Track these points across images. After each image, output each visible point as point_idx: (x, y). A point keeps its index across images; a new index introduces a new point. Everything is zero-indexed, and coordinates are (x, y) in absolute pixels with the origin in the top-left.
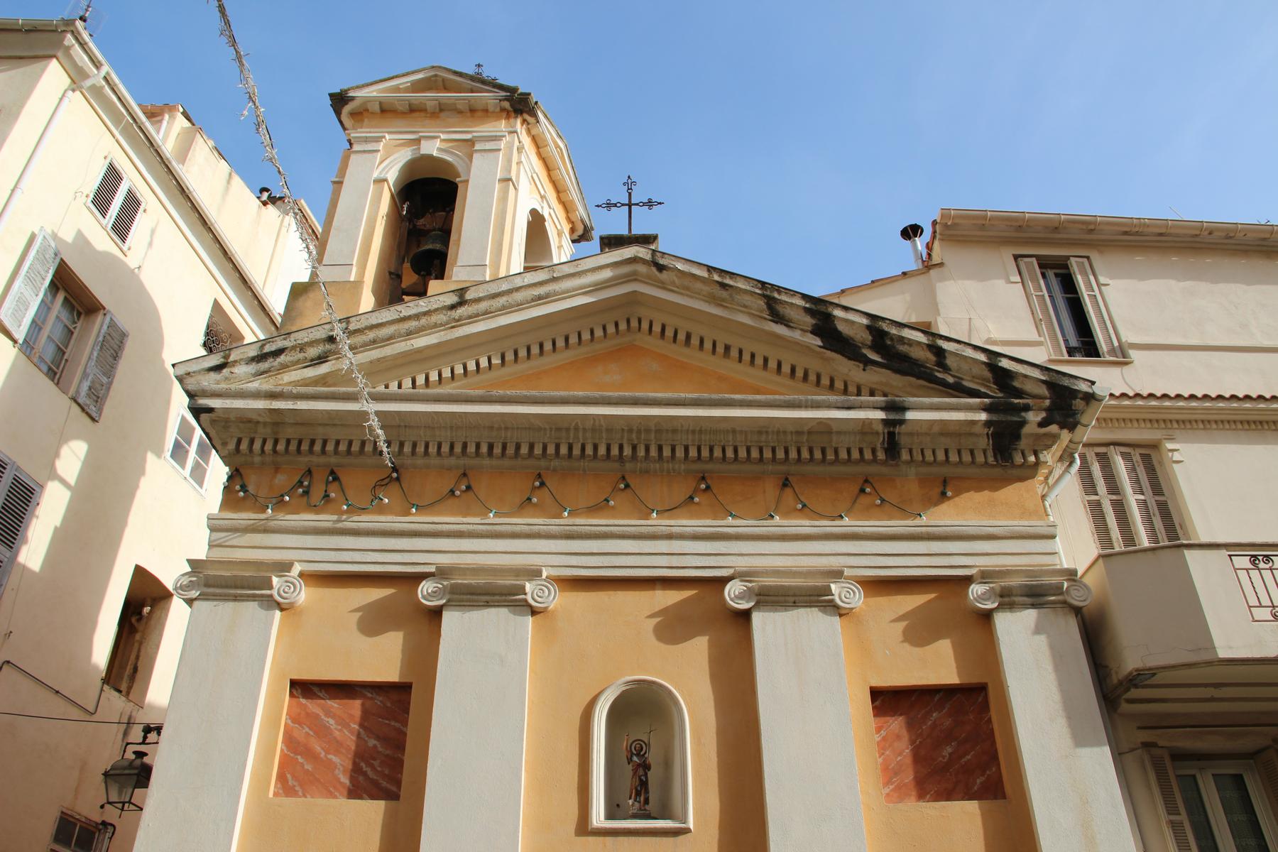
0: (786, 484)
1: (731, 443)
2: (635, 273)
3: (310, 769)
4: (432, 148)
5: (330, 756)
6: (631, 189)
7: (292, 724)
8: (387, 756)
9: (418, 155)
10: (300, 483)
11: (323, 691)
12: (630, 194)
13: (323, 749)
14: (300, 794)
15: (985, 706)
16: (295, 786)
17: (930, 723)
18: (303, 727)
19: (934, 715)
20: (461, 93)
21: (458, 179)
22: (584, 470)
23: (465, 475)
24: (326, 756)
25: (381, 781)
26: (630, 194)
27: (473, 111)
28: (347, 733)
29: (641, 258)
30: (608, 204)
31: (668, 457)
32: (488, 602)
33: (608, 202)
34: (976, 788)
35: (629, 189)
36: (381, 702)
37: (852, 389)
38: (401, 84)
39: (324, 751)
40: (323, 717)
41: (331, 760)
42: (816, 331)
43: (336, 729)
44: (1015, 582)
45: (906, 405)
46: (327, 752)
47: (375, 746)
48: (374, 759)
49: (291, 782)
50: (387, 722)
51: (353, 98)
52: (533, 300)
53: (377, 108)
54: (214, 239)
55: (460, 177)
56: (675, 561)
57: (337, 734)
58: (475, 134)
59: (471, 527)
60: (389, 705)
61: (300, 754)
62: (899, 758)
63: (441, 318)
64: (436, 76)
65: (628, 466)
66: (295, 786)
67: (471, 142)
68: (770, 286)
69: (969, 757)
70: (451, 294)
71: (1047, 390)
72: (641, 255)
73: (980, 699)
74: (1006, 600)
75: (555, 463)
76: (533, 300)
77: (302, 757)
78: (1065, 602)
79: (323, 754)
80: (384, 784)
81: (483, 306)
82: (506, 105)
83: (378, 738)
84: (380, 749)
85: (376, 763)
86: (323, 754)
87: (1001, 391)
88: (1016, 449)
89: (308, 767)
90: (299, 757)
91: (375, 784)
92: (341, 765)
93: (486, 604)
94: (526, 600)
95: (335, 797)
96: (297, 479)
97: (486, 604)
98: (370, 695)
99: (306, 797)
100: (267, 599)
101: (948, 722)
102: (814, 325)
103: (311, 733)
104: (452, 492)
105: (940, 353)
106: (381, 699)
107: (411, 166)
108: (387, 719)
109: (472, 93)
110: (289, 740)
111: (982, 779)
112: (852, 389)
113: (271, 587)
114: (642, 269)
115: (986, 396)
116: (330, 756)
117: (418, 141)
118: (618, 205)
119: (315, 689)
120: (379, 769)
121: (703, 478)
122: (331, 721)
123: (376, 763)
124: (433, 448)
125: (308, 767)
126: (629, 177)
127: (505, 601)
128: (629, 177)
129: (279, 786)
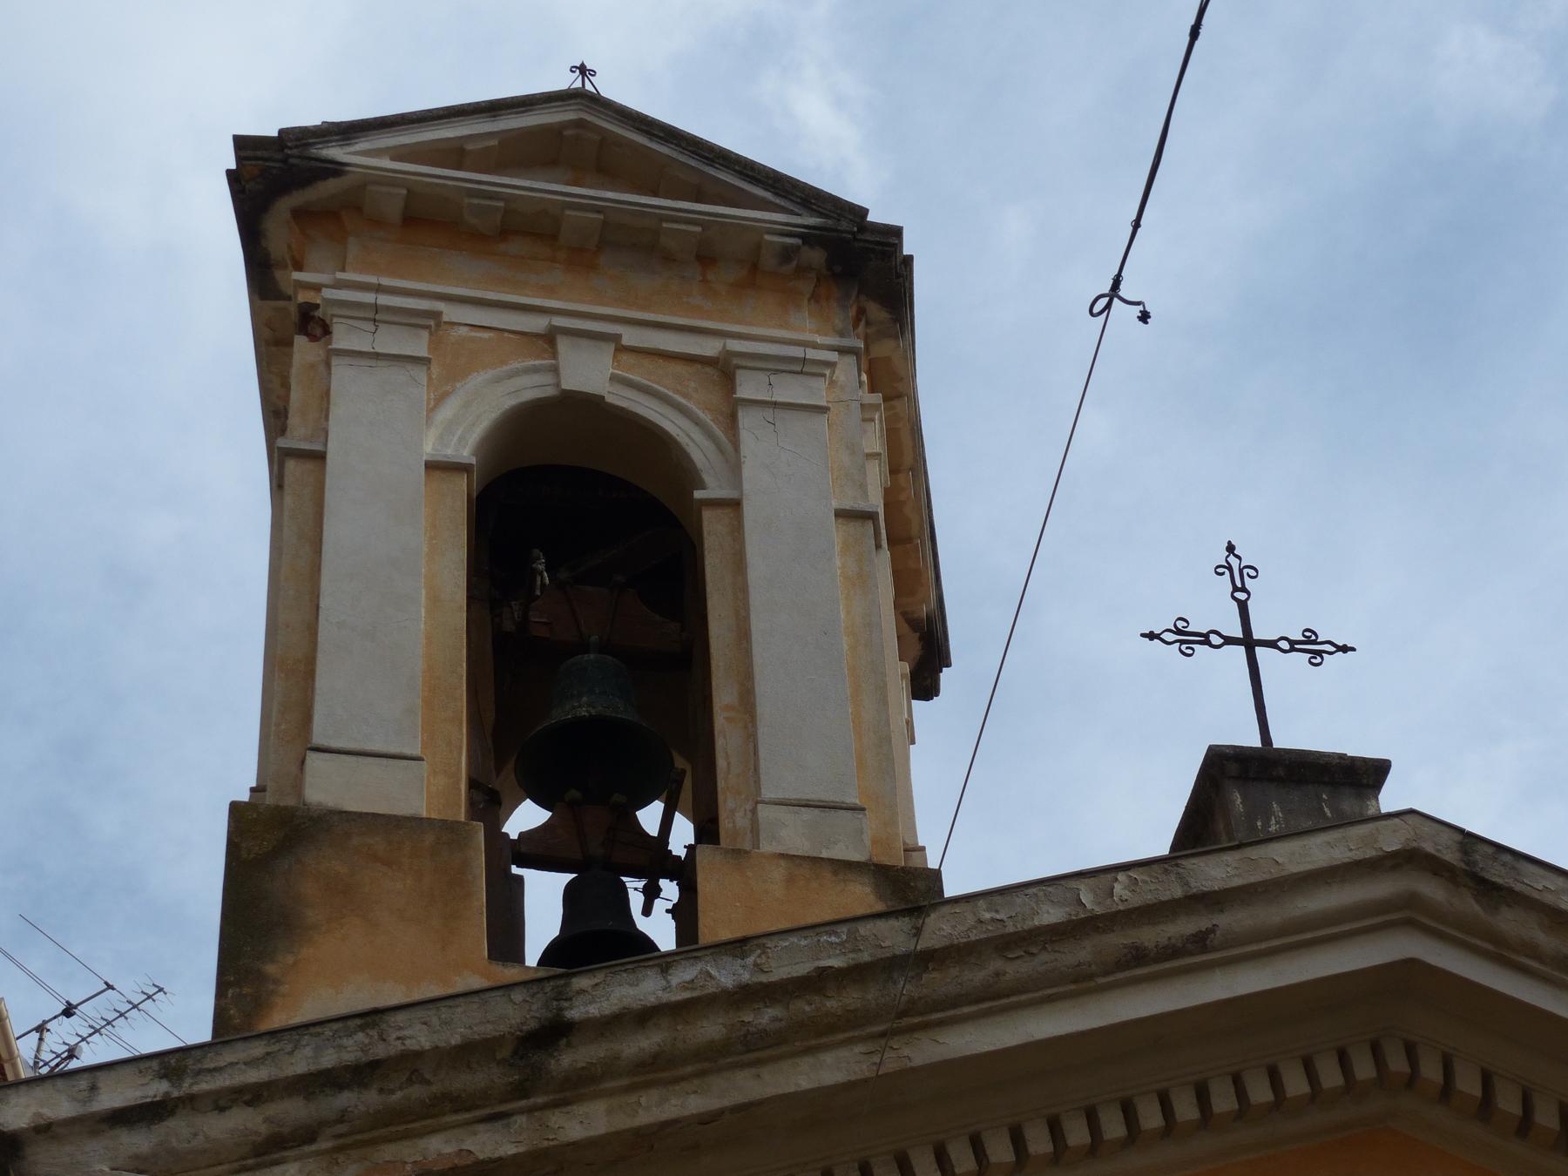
2: (1411, 901)
6: (1244, 589)
9: (550, 392)
12: (1243, 607)
20: (655, 194)
21: (698, 494)
26: (1243, 607)
27: (706, 257)
30: (1179, 632)
31: (609, 1112)
33: (1180, 624)
35: (1235, 589)
38: (470, 137)
51: (336, 169)
52: (1121, 965)
53: (393, 210)
54: (717, 950)
55: (702, 486)
58: (736, 346)
64: (580, 124)
67: (724, 370)
71: (1478, 902)
76: (1121, 965)
82: (816, 257)
109: (698, 201)
114: (1432, 890)
118: (1215, 640)
126: (1231, 548)
128: (1231, 548)
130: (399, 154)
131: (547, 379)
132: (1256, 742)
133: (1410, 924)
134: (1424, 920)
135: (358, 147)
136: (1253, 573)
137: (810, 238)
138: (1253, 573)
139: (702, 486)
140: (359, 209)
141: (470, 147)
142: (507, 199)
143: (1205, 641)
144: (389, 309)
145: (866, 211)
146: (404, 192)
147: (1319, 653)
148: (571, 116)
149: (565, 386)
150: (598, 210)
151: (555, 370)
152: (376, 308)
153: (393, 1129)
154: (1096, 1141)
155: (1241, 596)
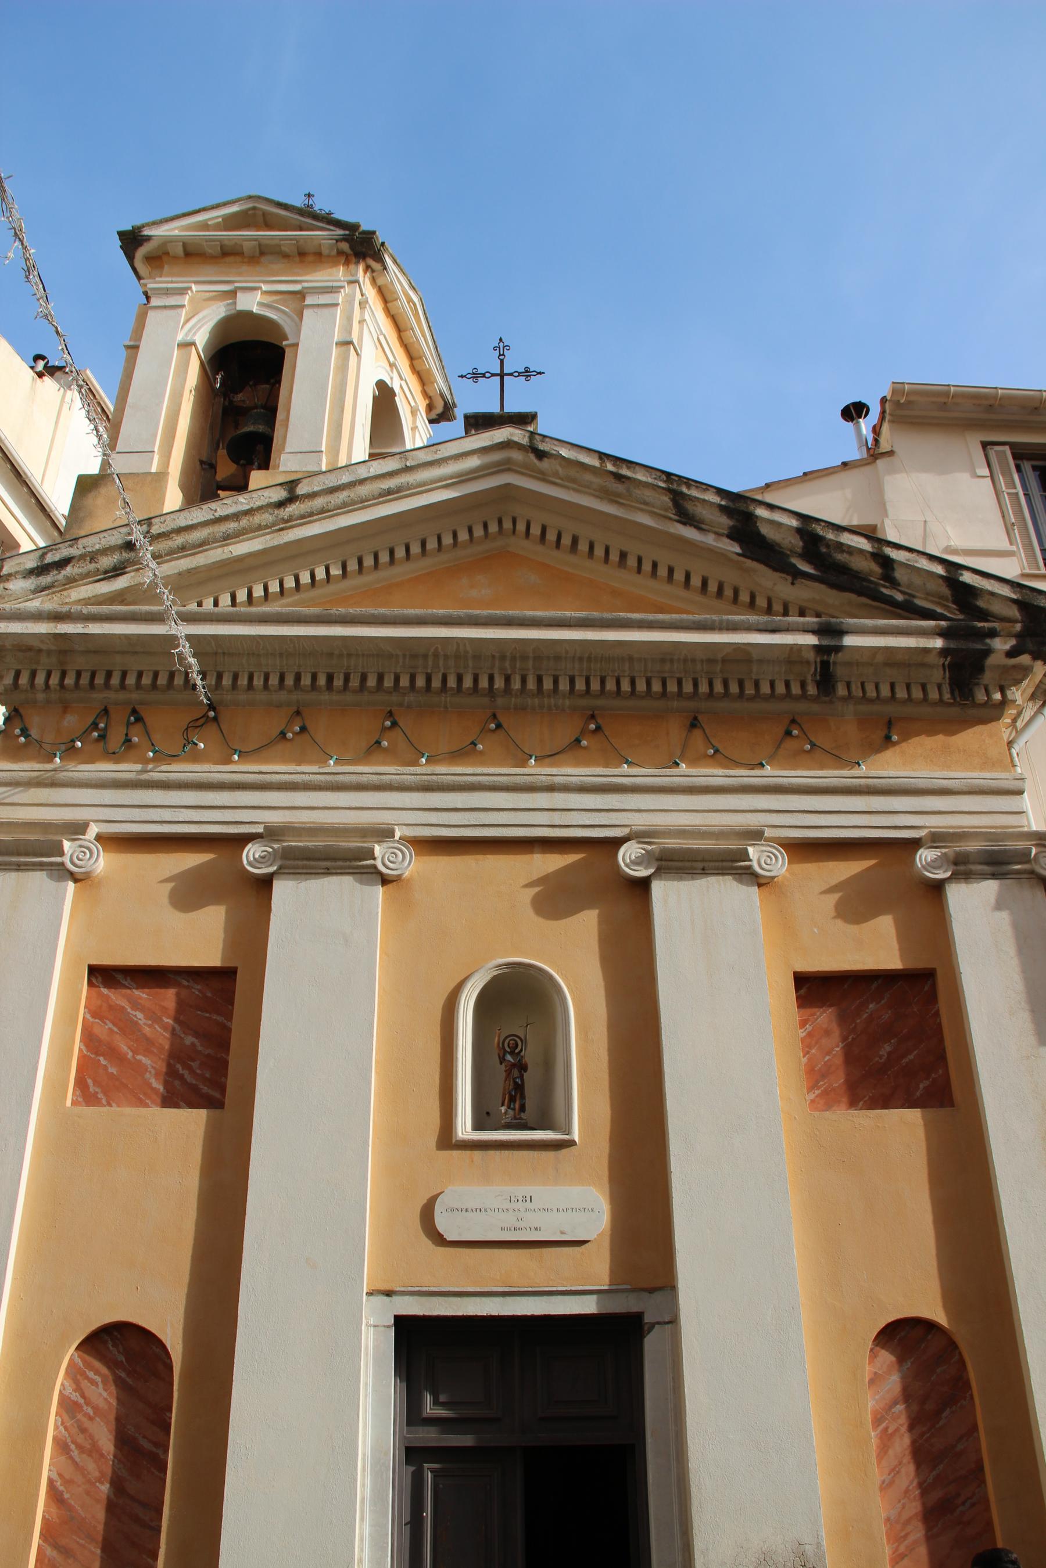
0: (694, 724)
1: (626, 674)
2: (508, 461)
3: (115, 1073)
4: (251, 302)
5: (139, 1057)
6: (503, 355)
7: (91, 1019)
8: (208, 1056)
9: (233, 312)
10: (95, 726)
11: (128, 978)
12: (502, 362)
13: (129, 1048)
14: (104, 1102)
15: (932, 997)
16: (97, 1093)
17: (865, 1015)
18: (105, 1023)
19: (871, 1006)
21: (284, 343)
22: (446, 707)
23: (298, 713)
24: (133, 1057)
25: (201, 1086)
26: (502, 362)
28: (159, 1030)
29: (516, 443)
30: (474, 374)
32: (19, 866)
33: (474, 371)
34: (918, 1094)
35: (500, 355)
36: (200, 991)
37: (777, 607)
38: (210, 219)
39: (132, 1051)
40: (129, 1010)
41: (140, 1061)
42: (733, 535)
43: (145, 1024)
44: (972, 846)
45: (844, 628)
46: (135, 1052)
47: (193, 1044)
48: (194, 1060)
49: (92, 1089)
50: (207, 1015)
51: (148, 238)
52: (381, 495)
53: (179, 251)
55: (287, 339)
56: (557, 818)
57: (147, 1030)
58: (306, 285)
59: (306, 778)
60: (209, 994)
61: (102, 1055)
62: (827, 1058)
63: (266, 518)
64: (254, 208)
65: (500, 701)
66: (97, 1093)
67: (301, 295)
68: (676, 479)
69: (911, 1057)
70: (278, 488)
72: (516, 439)
73: (926, 988)
74: (962, 868)
75: (411, 698)
76: (381, 495)
77: (105, 1059)
78: (1032, 872)
79: (130, 1055)
80: (205, 1089)
81: (319, 502)
83: (197, 1035)
84: (200, 1048)
85: (195, 1065)
86: (130, 1055)
87: (961, 611)
88: (978, 684)
89: (112, 1070)
90: (101, 1059)
91: (194, 1089)
92: (152, 1067)
93: (326, 871)
94: (375, 867)
95: (146, 1106)
96: (91, 720)
97: (326, 871)
98: (185, 983)
99: (109, 1105)
100: (57, 868)
101: (887, 1016)
102: (732, 528)
103: (116, 1029)
104: (283, 734)
105: (887, 563)
106: (199, 987)
107: (225, 326)
108: (207, 1012)
110: (89, 1037)
111: (927, 1083)
112: (777, 607)
113: (62, 854)
114: (517, 455)
115: (941, 617)
116: (139, 1057)
117: (233, 294)
118: (488, 375)
119: (119, 977)
120: (198, 1071)
121: (593, 717)
122: (140, 1015)
123: (195, 1065)
124: (259, 679)
125: (112, 1070)
126: (501, 340)
127: (350, 867)
128: (501, 340)
129: (78, 1093)
130: (189, 228)
131: (232, 307)
132: (499, 411)
133: (509, 470)
134: (514, 468)
135: (161, 230)
136: (508, 348)
137: (344, 239)
138: (508, 348)
139: (287, 339)
140: (167, 253)
141: (209, 223)
142: (220, 241)
143: (483, 375)
144: (172, 288)
145: (121, 246)
146: (181, 244)
147: (530, 376)
148: (251, 205)
149: (238, 309)
150: (256, 240)
151: (235, 303)
152: (167, 289)
153: (84, 581)
154: (727, 693)
155: (501, 357)
